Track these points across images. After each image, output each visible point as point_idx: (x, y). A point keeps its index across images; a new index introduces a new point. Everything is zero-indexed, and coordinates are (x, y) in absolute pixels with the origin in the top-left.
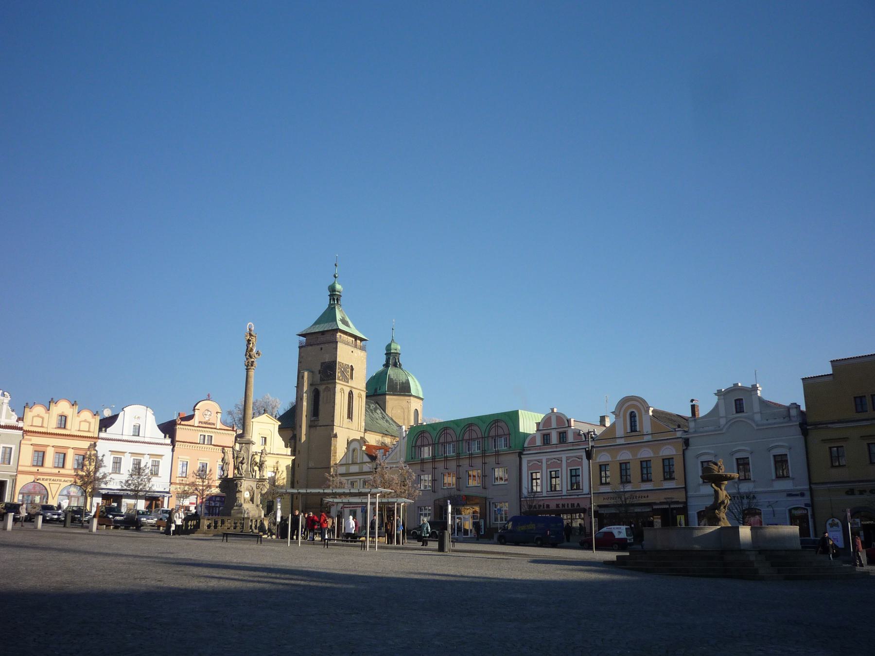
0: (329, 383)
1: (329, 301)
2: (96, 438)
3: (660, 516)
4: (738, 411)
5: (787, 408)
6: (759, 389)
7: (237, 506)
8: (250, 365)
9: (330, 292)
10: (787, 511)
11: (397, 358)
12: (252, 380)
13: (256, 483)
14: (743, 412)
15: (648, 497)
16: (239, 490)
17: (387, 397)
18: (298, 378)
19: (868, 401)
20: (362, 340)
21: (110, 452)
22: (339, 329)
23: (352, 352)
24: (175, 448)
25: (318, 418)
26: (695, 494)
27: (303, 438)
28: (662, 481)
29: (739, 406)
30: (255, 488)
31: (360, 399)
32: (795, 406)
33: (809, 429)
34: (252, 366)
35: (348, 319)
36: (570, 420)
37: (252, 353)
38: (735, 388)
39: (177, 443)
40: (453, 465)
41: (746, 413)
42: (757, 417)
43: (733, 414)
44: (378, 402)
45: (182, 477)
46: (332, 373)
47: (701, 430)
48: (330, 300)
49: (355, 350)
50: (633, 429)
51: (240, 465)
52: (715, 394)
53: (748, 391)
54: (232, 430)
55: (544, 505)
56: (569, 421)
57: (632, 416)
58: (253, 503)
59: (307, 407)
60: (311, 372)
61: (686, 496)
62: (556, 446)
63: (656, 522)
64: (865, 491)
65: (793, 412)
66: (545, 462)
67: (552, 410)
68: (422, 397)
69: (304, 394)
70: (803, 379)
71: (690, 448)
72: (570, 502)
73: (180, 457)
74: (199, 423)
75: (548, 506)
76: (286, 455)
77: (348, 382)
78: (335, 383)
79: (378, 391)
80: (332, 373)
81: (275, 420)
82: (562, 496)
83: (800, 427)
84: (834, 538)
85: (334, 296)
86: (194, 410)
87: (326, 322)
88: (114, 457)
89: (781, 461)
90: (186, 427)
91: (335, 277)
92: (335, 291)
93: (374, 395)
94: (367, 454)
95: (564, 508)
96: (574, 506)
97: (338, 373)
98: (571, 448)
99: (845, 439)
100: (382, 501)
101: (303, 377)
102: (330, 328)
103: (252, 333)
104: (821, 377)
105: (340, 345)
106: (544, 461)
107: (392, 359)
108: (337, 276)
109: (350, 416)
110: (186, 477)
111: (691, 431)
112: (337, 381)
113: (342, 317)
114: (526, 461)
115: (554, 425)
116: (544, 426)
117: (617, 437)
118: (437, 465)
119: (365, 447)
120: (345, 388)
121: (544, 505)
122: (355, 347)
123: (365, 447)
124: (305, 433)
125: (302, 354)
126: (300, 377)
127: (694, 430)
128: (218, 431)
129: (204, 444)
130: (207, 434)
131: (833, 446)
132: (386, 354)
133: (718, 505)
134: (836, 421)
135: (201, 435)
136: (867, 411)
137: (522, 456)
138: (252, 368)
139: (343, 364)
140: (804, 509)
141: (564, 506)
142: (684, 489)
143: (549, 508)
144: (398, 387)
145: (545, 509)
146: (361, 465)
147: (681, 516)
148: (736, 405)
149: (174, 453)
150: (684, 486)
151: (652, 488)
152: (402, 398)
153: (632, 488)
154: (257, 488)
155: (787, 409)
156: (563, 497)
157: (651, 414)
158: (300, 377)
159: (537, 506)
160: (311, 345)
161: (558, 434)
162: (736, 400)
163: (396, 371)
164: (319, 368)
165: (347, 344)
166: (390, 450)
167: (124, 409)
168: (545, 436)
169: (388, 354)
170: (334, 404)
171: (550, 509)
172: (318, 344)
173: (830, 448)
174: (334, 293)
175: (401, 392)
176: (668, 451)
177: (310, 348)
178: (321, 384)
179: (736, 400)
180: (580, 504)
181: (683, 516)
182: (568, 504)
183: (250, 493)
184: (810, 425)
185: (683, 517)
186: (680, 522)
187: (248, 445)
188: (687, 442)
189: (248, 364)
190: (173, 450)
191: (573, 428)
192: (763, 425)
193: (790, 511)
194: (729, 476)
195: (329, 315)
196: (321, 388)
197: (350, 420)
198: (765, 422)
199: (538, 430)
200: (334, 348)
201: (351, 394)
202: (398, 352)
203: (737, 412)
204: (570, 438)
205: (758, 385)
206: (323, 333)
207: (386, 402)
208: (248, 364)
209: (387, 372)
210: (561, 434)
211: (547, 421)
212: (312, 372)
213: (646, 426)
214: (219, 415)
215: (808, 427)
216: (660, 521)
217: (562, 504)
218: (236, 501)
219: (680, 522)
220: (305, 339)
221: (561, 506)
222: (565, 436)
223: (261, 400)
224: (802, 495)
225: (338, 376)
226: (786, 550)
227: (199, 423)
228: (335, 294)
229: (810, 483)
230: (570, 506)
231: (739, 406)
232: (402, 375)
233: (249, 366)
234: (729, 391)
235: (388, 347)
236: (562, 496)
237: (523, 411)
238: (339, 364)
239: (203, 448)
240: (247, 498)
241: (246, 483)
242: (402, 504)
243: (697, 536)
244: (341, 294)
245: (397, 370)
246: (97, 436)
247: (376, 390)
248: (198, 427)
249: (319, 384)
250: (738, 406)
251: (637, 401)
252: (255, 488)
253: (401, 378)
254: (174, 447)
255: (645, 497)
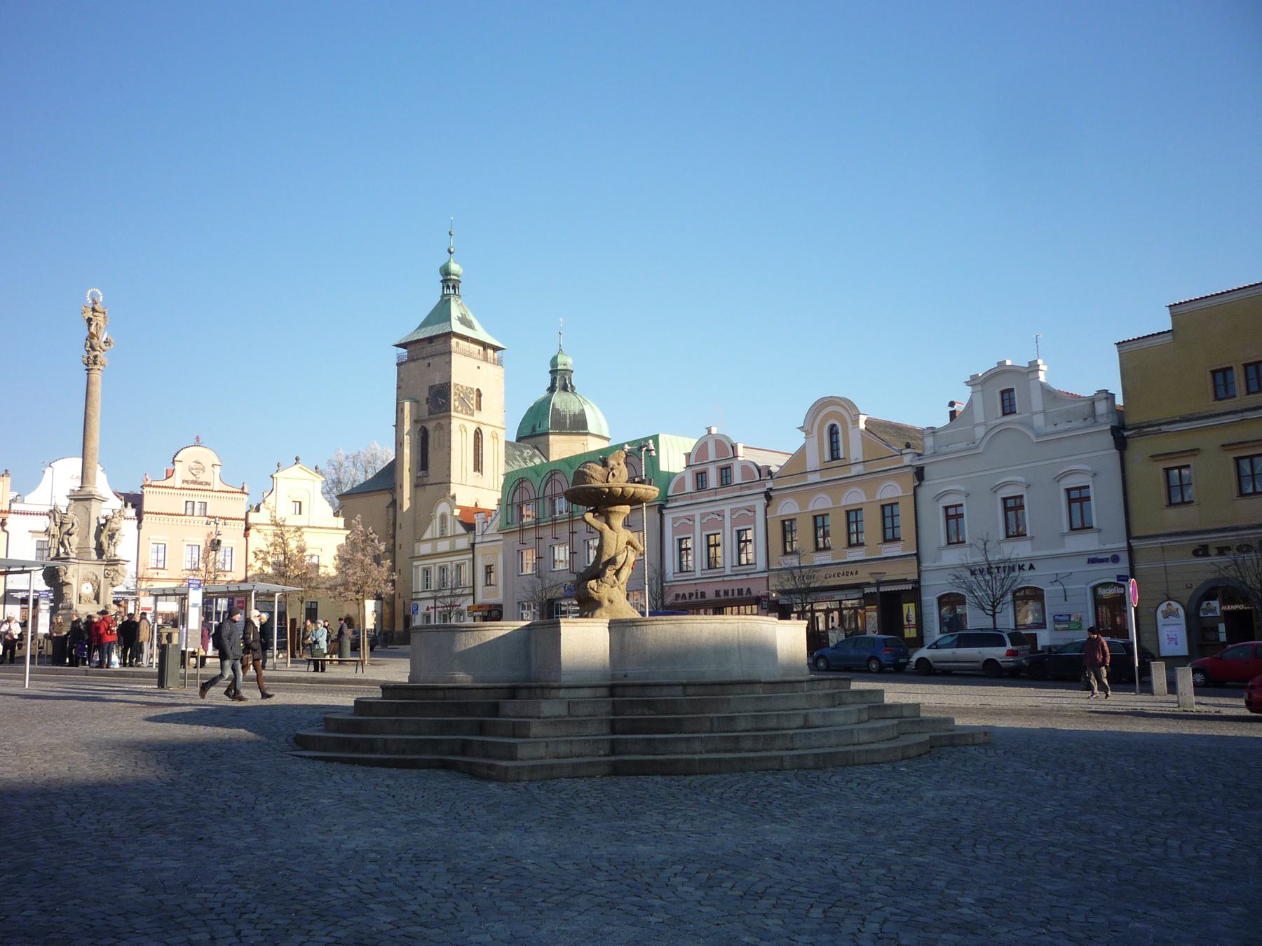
0: (440, 418)
1: (441, 290)
2: (5, 512)
3: (875, 607)
4: (1006, 412)
5: (1090, 400)
6: (1041, 368)
7: (63, 609)
8: (91, 362)
9: (443, 276)
10: (1089, 589)
11: (567, 377)
12: (97, 390)
13: (103, 567)
14: (1015, 412)
15: (857, 573)
16: (63, 581)
17: (551, 438)
18: (397, 412)
19: (1238, 376)
20: (496, 349)
21: (30, 533)
22: (452, 332)
23: (479, 368)
24: (142, 523)
25: (427, 473)
26: (933, 564)
27: (406, 505)
28: (879, 544)
29: (1008, 403)
30: (102, 578)
31: (496, 440)
32: (1104, 395)
33: (1128, 437)
34: (95, 364)
35: (471, 317)
36: (737, 446)
37: (95, 341)
38: (1001, 371)
39: (145, 516)
40: (563, 531)
41: (1020, 414)
42: (1039, 421)
43: (997, 419)
44: (538, 446)
45: (157, 568)
46: (444, 401)
47: (944, 449)
48: (443, 288)
49: (484, 365)
50: (834, 456)
51: (66, 536)
52: (966, 382)
53: (1022, 373)
54: (240, 493)
55: (697, 593)
56: (734, 447)
57: (833, 431)
58: (98, 603)
59: (410, 455)
60: (415, 401)
61: (918, 569)
62: (716, 492)
63: (870, 617)
64: (1228, 548)
65: (1102, 407)
66: (699, 521)
67: (709, 430)
68: (609, 437)
69: (405, 436)
70: (1118, 344)
71: (923, 483)
72: (736, 587)
73: (151, 537)
74: (183, 483)
75: (703, 594)
76: (337, 529)
77: (472, 415)
78: (449, 417)
79: (537, 429)
80: (444, 401)
81: (315, 474)
82: (723, 576)
83: (1112, 434)
84: (1170, 637)
85: (448, 281)
86: (173, 462)
87: (436, 324)
88: (38, 541)
89: (1078, 498)
90: (161, 490)
91: (450, 253)
92: (450, 274)
93: (531, 436)
94: (461, 522)
95: (749, 595)
96: (742, 592)
97: (455, 400)
98: (739, 494)
99: (1194, 452)
100: (241, 589)
101: (402, 410)
102: (441, 332)
103: (97, 307)
104: (1151, 338)
105: (455, 358)
106: (697, 518)
107: (560, 379)
108: (452, 250)
109: (478, 466)
110: (164, 569)
111: (928, 452)
112: (453, 413)
113: (462, 314)
114: (671, 519)
115: (712, 457)
116: (696, 458)
117: (808, 470)
118: (543, 533)
119: (459, 511)
120: (467, 424)
121: (697, 593)
122: (484, 361)
123: (459, 511)
124: (408, 496)
125: (402, 376)
126: (400, 410)
127: (932, 451)
128: (217, 494)
129: (193, 515)
130: (196, 500)
131: (1172, 466)
132: (551, 372)
133: (601, 567)
134: (1178, 419)
135: (187, 502)
136: (1235, 396)
137: (664, 512)
138: (96, 367)
139: (462, 386)
140: (1115, 584)
141: (740, 591)
142: (915, 557)
143: (705, 597)
144: (568, 421)
145: (700, 599)
146: (453, 538)
147: (909, 604)
148: (1003, 400)
149: (141, 530)
150: (916, 552)
151: (865, 558)
152: (574, 438)
153: (866, 556)
154: (105, 577)
155: (1090, 402)
156: (725, 579)
157: (862, 426)
158: (400, 411)
159: (687, 596)
160: (414, 360)
161: (719, 471)
162: (1003, 393)
163: (565, 397)
164: (426, 394)
165: (469, 355)
166: (493, 513)
167: (52, 465)
168: (700, 476)
169: (554, 372)
170: (450, 450)
171: (707, 599)
172: (424, 358)
173: (1167, 470)
174: (449, 277)
175: (573, 429)
176: (892, 490)
177: (412, 365)
178: (430, 420)
179: (1003, 393)
180: (751, 589)
181: (913, 604)
182: (733, 590)
183: (93, 585)
184: (1130, 430)
185: (912, 606)
186: (908, 615)
187: (87, 502)
188: (920, 473)
189: (88, 361)
190: (139, 527)
191: (743, 459)
192: (1047, 435)
193: (1095, 589)
194: (607, 490)
195: (441, 312)
196: (430, 426)
197: (480, 474)
198: (1050, 429)
199: (688, 466)
200: (447, 363)
201: (478, 434)
202: (569, 368)
203: (1004, 414)
204: (737, 478)
205: (1040, 362)
206: (430, 340)
207: (549, 445)
208: (88, 361)
209: (551, 400)
210: (724, 471)
211: (701, 449)
212: (417, 402)
213: (854, 449)
214: (217, 469)
215: (1126, 434)
216: (875, 614)
217: (725, 591)
218: (63, 599)
219: (908, 615)
220: (406, 350)
221: (722, 593)
222: (728, 474)
223: (366, 452)
224: (1115, 559)
225: (454, 406)
226: (685, 686)
227: (183, 483)
228: (450, 280)
229: (1129, 536)
230: (736, 593)
231: (1008, 403)
232: (574, 402)
233: (90, 363)
234: (991, 376)
235: (554, 362)
236: (724, 576)
237: (667, 436)
238: (455, 387)
239: (196, 522)
240: (86, 596)
241: (83, 569)
242: (277, 595)
243: (463, 648)
244: (460, 279)
245: (567, 397)
246: (7, 509)
247: (534, 428)
248: (181, 489)
249: (427, 420)
250: (1007, 403)
251: (839, 405)
252: (102, 578)
253: (572, 407)
254: (140, 521)
255: (852, 574)
